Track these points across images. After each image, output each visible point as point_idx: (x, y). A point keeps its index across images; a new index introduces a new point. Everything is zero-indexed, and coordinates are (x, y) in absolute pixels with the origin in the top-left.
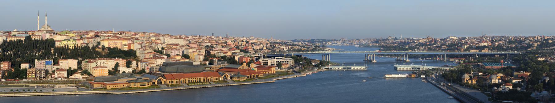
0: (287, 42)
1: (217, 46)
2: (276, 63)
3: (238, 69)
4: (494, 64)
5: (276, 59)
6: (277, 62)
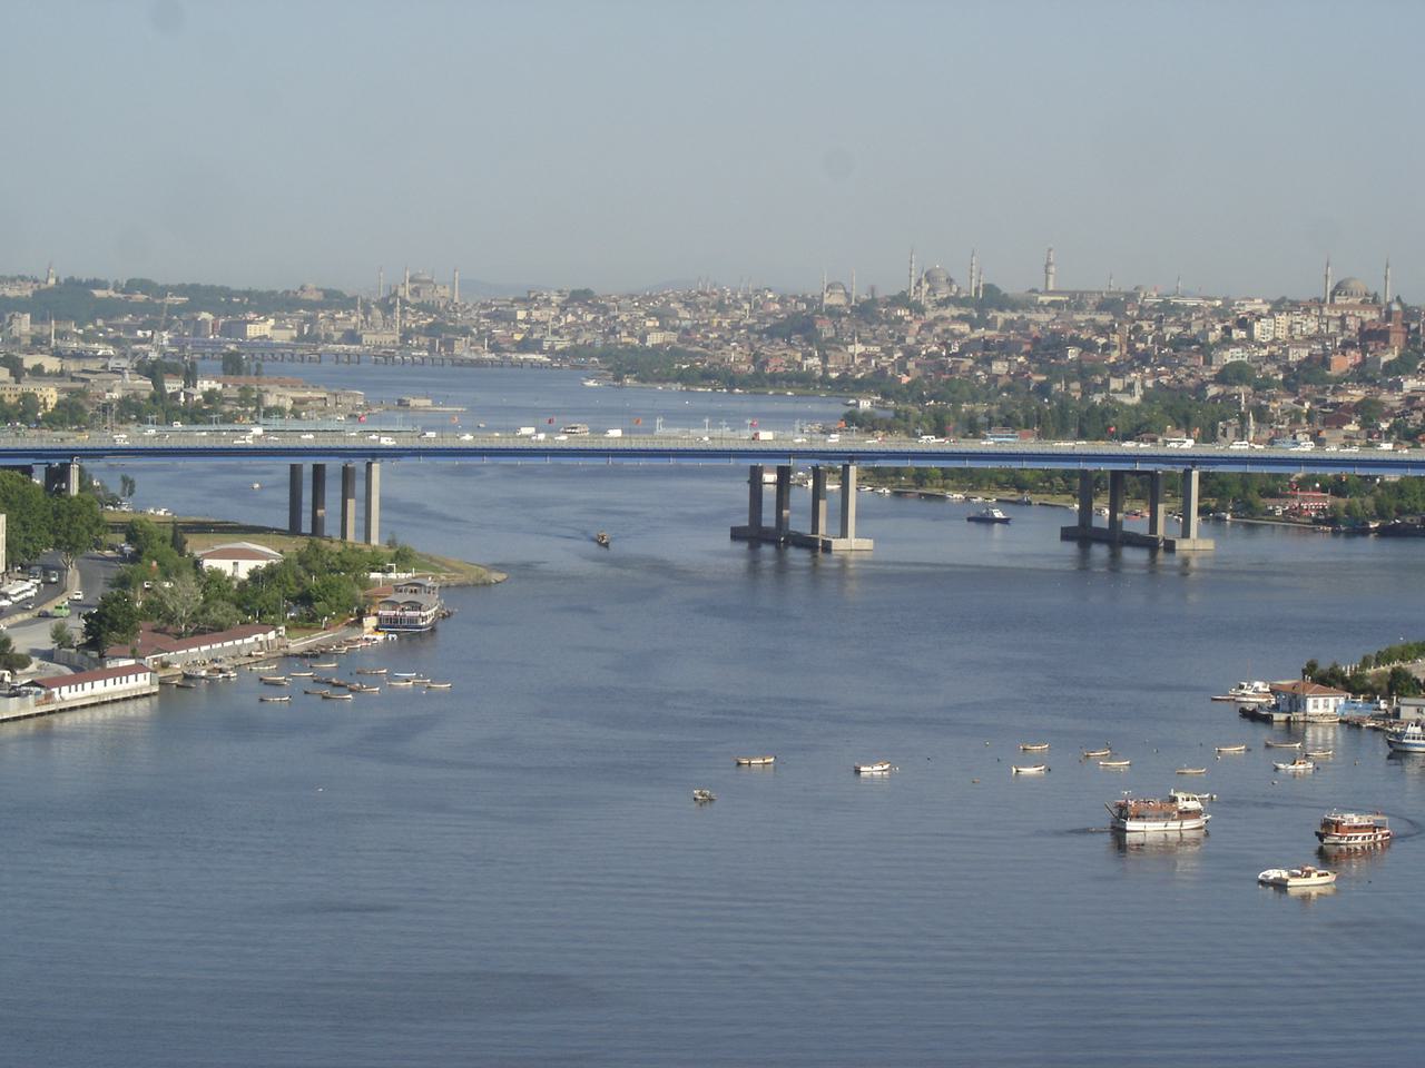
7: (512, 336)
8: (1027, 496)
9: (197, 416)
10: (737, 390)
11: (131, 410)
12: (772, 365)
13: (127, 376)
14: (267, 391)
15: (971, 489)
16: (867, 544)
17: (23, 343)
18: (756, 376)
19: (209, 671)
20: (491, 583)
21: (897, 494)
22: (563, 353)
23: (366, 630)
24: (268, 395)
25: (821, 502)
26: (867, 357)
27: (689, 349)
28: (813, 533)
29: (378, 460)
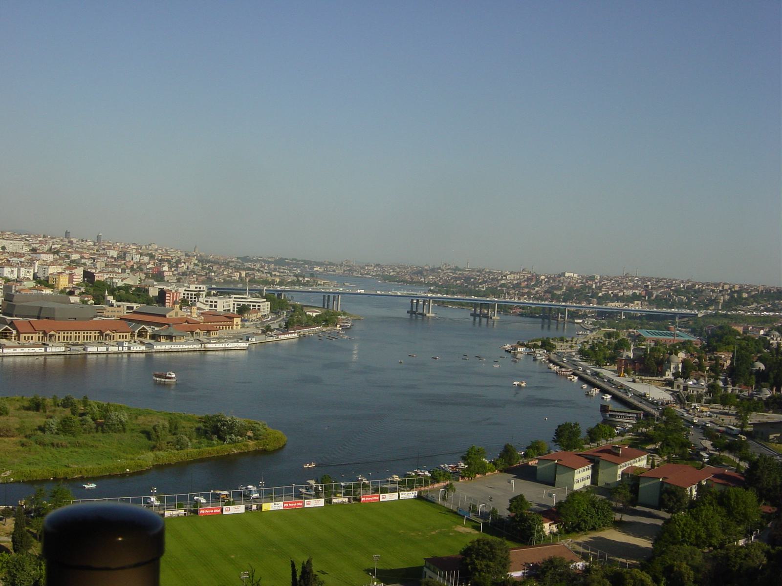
0: (230, 262)
1: (94, 261)
2: (234, 308)
3: (165, 316)
4: (655, 332)
5: (233, 299)
6: (236, 306)
11: (293, 283)
25: (157, 295)
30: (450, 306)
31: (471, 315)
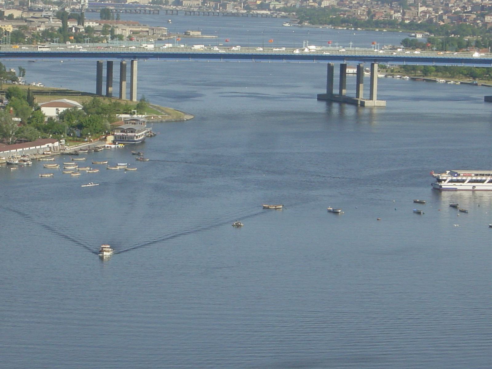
7: (256, 2)
8: (477, 81)
9: (79, 39)
10: (359, 29)
11: (47, 36)
12: (377, 16)
13: (51, 20)
14: (117, 27)
15: (448, 78)
16: (383, 103)
17: (16, 4)
18: (368, 22)
19: (19, 161)
20: (184, 120)
21: (413, 79)
22: (279, 10)
23: (107, 142)
24: (117, 29)
25: (360, 84)
26: (425, 13)
27: (342, 9)
28: (357, 98)
29: (137, 59)
30: (442, 81)
31: (320, 98)
